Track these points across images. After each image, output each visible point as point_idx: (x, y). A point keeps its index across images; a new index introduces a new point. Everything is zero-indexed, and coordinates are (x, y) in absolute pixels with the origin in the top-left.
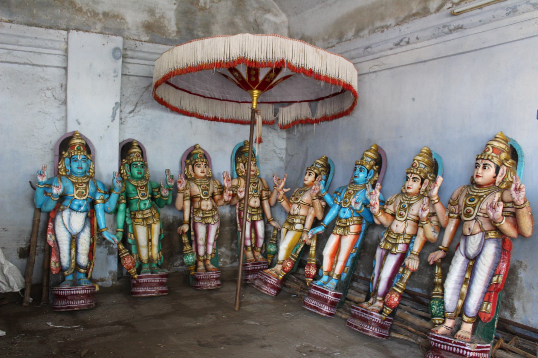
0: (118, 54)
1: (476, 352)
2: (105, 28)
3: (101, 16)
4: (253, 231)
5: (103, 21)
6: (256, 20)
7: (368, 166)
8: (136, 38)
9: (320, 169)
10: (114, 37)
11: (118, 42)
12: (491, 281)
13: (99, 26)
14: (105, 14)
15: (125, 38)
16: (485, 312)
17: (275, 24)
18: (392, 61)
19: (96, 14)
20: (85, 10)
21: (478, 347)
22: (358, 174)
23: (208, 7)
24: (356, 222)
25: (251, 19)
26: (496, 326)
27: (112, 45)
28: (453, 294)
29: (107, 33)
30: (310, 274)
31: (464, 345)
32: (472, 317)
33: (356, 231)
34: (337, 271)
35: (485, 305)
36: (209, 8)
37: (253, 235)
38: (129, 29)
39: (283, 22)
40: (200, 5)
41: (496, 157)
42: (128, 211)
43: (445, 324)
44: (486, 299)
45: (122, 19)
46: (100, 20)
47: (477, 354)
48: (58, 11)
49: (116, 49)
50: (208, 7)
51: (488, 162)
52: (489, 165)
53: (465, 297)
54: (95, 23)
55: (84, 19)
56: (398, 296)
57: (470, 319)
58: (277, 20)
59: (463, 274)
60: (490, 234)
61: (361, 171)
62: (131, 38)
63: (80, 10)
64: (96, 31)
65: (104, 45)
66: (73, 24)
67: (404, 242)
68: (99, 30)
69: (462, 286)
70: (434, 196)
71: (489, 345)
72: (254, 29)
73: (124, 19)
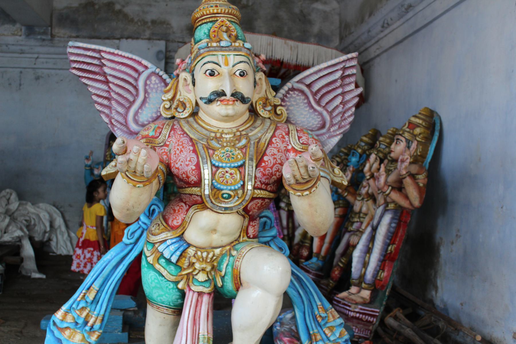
0: (162, 56)
1: (360, 313)
2: (153, 34)
3: (150, 24)
4: (290, 220)
5: (151, 27)
6: (302, 11)
7: (360, 151)
8: (181, 40)
9: (343, 157)
10: (158, 42)
11: (161, 45)
12: (387, 250)
13: (148, 33)
14: (154, 22)
15: (167, 41)
16: (379, 280)
17: (325, 12)
18: (385, 43)
19: (145, 23)
20: (136, 20)
21: (361, 309)
22: (350, 159)
23: (250, 4)
24: (341, 205)
25: (297, 10)
26: (387, 293)
27: (156, 49)
28: (358, 262)
29: (155, 38)
30: (302, 256)
31: (350, 306)
32: (368, 284)
33: (341, 214)
34: (323, 253)
35: (380, 273)
36: (252, 5)
37: (290, 225)
38: (174, 33)
39: (334, 9)
40: (242, 3)
41: (408, 132)
42: (165, 194)
43: (350, 291)
44: (382, 268)
45: (168, 24)
46: (149, 28)
47: (361, 315)
48: (114, 24)
49: (160, 52)
50: (250, 4)
51: (400, 137)
52: (401, 141)
53: (365, 265)
54: (144, 31)
55: (135, 28)
56: (339, 269)
57: (366, 286)
58: (327, 8)
59: (368, 244)
60: (389, 206)
61: (353, 155)
62: (176, 40)
63: (132, 20)
64: (145, 37)
65: (149, 49)
66: (126, 34)
67: (358, 220)
68: (147, 36)
69: (366, 256)
70: (366, 173)
71: (378, 310)
72: (300, 20)
73: (170, 25)
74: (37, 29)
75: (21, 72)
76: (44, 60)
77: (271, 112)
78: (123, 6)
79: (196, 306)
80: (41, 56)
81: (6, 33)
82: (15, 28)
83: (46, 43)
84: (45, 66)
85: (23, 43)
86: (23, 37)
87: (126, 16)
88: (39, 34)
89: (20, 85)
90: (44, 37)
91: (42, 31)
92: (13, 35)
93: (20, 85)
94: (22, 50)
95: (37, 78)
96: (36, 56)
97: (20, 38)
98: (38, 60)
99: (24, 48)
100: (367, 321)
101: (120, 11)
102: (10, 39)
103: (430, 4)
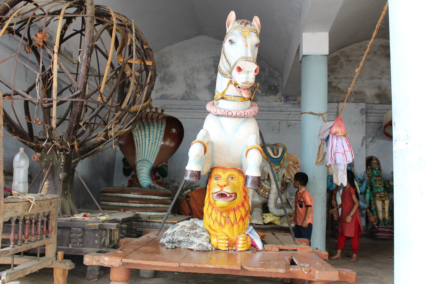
0: (363, 112)
8: (372, 102)
10: (361, 104)
11: (363, 106)
27: (360, 108)
38: (368, 98)
45: (364, 93)
46: (353, 96)
49: (362, 110)
68: (353, 101)
74: (290, 98)
75: (279, 123)
76: (294, 115)
77: (220, 97)
78: (338, 84)
79: (185, 109)
80: (292, 113)
81: (271, 100)
82: (276, 98)
83: (296, 105)
84: (294, 119)
85: (282, 106)
86: (282, 102)
87: (339, 89)
88: (292, 100)
89: (279, 130)
90: (294, 102)
91: (293, 99)
92: (276, 101)
93: (279, 130)
94: (281, 110)
95: (289, 126)
96: (289, 113)
97: (281, 103)
98: (290, 115)
99: (282, 109)
100: (150, 80)
101: (336, 87)
102: (275, 104)
103: (7, 86)
